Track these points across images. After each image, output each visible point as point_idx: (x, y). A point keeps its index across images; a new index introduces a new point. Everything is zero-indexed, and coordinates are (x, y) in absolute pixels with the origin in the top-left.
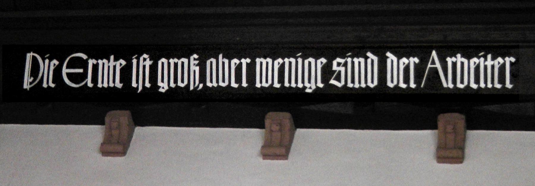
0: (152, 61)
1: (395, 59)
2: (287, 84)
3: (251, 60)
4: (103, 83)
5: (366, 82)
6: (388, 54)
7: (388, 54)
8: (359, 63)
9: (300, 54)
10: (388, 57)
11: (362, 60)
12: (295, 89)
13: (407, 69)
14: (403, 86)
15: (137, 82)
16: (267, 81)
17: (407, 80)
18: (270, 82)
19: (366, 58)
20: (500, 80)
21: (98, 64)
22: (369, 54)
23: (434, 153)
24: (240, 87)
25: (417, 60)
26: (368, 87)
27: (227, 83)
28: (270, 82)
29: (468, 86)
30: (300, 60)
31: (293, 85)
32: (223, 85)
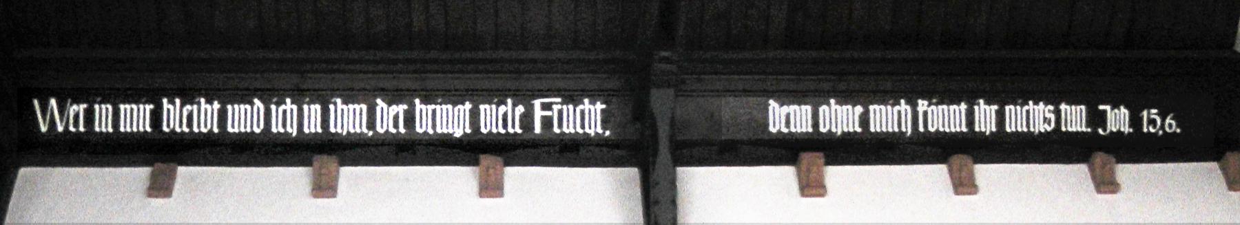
0: (771, 102)
1: (385, 106)
2: (196, 130)
3: (522, 104)
4: (125, 127)
5: (252, 127)
6: (379, 101)
7: (379, 101)
8: (246, 110)
9: (36, 102)
10: (1028, 104)
11: (248, 107)
12: (262, 136)
13: (396, 118)
14: (394, 131)
15: (986, 127)
16: (206, 126)
17: (396, 126)
18: (209, 126)
19: (252, 104)
20: (326, 123)
21: (562, 109)
22: (256, 101)
23: (690, 203)
24: (78, 131)
25: (405, 107)
26: (253, 132)
27: (385, 128)
28: (209, 126)
29: (387, 131)
30: (494, 107)
31: (104, 130)
32: (204, 130)
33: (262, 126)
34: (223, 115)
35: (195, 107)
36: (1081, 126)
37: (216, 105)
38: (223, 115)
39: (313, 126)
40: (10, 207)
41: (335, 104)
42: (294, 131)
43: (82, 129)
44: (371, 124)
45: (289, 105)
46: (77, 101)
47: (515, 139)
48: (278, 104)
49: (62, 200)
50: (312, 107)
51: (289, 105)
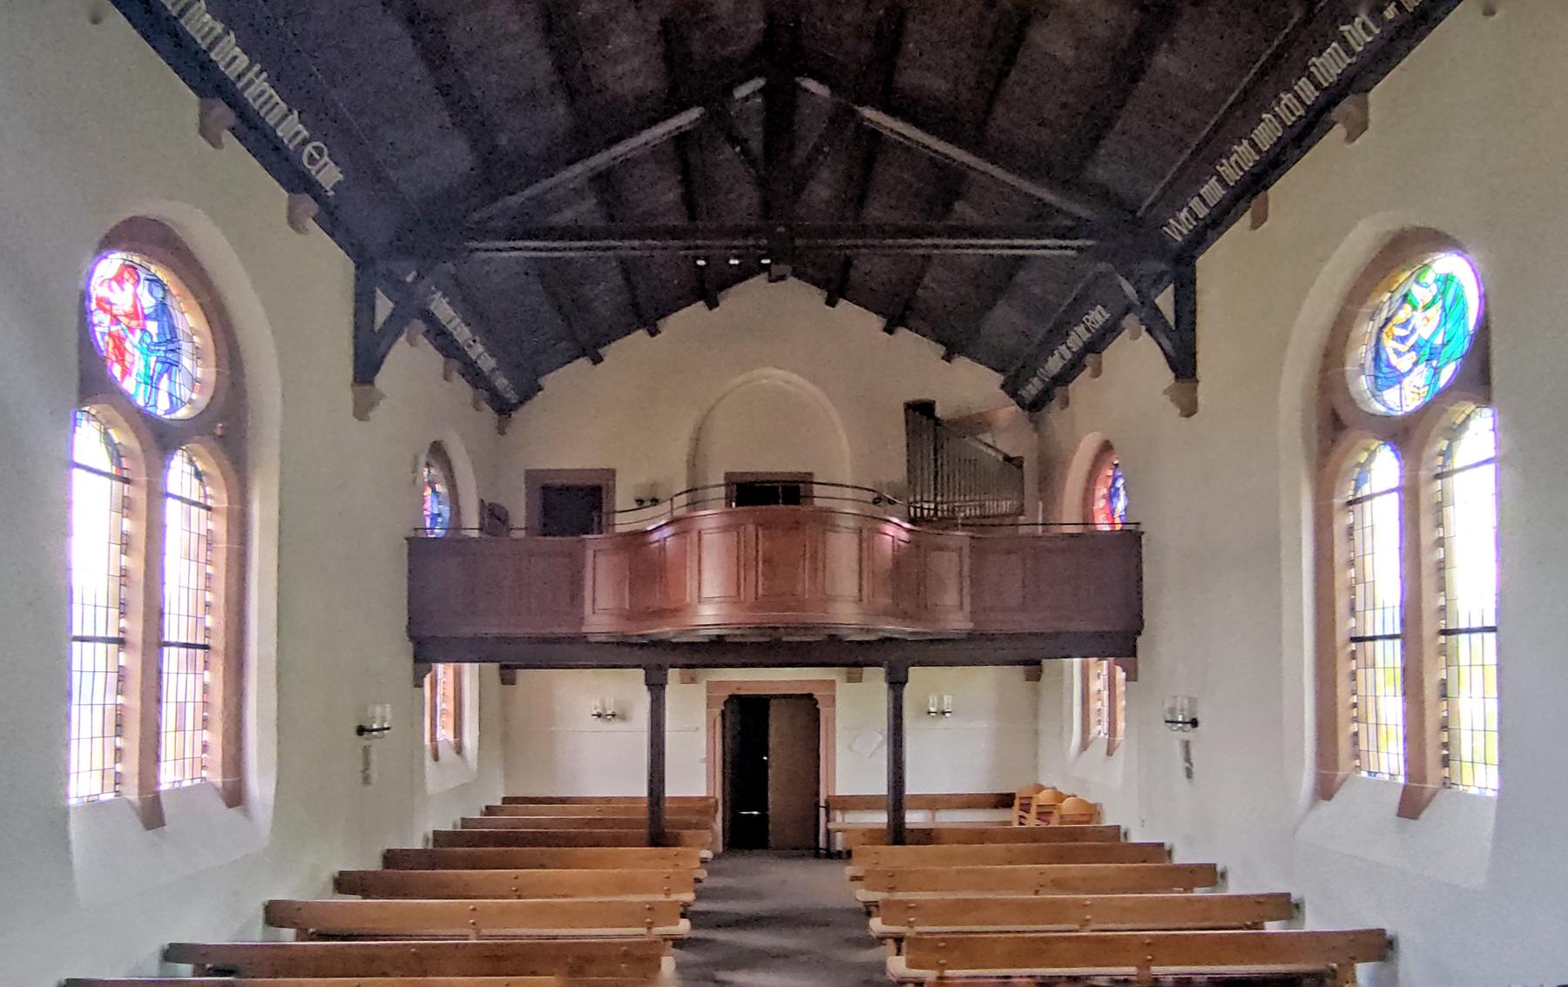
7: (1342, 28)
19: (1262, 120)
33: (1281, 129)
34: (1254, 145)
35: (1235, 155)
36: (1343, 61)
37: (1245, 142)
38: (1254, 145)
39: (1309, 93)
40: (1066, 502)
41: (1314, 65)
42: (1302, 112)
43: (1377, 31)
44: (1349, 51)
45: (1286, 98)
46: (1180, 210)
47: (834, 527)
48: (1279, 103)
49: (523, 50)
50: (1300, 83)
51: (1286, 98)
